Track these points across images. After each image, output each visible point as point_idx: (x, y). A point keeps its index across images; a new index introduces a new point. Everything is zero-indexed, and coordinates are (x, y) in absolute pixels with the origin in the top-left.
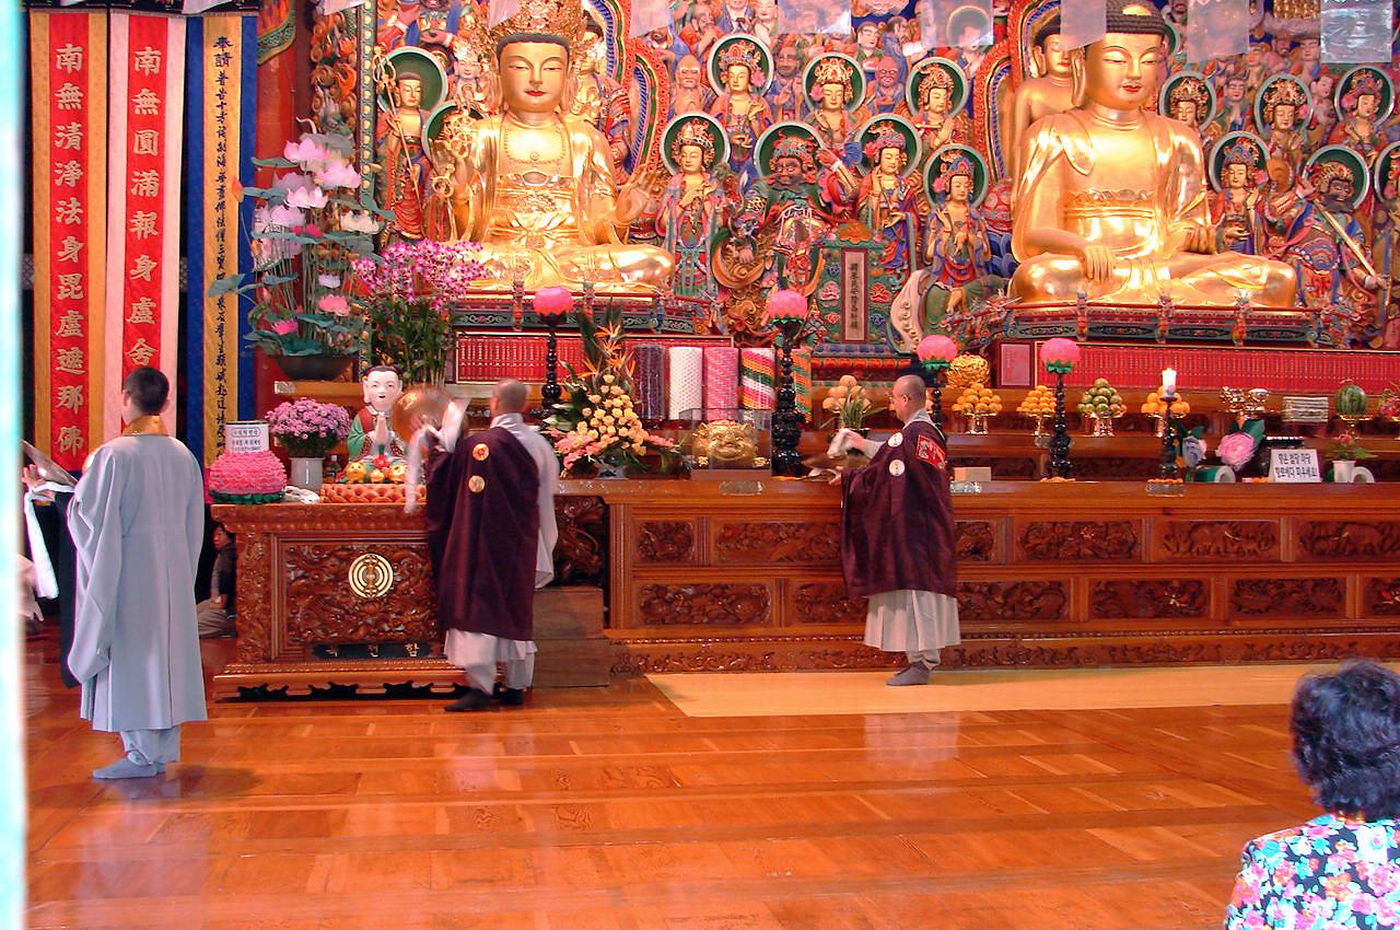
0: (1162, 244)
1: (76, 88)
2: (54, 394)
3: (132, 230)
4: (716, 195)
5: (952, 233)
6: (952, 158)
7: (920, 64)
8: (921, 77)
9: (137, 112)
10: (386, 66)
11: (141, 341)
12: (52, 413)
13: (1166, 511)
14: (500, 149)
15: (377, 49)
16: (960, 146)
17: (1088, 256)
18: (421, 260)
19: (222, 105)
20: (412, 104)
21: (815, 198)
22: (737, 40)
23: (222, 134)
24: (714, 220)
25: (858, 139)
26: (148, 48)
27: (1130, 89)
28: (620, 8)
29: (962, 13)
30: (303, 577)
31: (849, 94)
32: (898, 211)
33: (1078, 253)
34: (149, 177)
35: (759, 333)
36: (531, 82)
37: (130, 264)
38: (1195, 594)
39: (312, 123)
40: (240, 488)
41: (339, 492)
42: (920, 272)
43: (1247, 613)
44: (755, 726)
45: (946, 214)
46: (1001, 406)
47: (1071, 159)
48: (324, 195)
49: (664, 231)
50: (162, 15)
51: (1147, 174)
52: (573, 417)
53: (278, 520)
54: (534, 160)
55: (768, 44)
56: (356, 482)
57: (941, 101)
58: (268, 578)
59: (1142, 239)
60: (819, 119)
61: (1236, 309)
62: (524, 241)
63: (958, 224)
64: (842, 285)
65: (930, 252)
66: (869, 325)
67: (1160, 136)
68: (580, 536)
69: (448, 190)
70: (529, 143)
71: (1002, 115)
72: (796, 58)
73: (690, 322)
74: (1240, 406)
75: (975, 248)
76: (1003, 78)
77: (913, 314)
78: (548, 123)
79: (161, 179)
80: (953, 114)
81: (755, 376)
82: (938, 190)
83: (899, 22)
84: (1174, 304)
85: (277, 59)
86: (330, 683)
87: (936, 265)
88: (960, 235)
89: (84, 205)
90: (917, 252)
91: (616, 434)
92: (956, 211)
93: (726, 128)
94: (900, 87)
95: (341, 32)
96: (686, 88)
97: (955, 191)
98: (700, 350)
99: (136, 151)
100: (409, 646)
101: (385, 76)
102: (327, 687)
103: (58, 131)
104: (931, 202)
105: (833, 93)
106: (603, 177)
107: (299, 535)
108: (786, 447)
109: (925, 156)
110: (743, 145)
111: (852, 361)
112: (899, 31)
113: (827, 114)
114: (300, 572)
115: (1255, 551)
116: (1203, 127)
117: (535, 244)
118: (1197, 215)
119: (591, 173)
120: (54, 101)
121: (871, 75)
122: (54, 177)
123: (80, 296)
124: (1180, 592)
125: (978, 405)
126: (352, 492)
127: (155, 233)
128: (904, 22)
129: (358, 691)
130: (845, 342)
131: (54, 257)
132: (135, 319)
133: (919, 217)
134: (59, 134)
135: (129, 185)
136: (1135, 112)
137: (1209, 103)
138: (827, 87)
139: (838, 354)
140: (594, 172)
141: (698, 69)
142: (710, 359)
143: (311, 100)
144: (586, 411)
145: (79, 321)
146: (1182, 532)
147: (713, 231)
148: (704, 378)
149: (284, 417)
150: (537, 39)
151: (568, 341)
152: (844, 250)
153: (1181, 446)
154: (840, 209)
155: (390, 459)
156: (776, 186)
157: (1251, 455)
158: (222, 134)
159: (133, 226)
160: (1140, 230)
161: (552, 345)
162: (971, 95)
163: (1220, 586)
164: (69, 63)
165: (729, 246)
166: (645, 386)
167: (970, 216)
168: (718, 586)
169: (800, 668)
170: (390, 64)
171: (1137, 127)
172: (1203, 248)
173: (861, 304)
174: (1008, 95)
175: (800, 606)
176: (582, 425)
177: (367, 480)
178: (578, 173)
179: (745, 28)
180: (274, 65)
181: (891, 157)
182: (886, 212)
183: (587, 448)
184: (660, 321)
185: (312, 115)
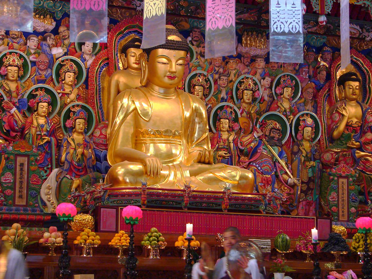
5: (75, 149)
8: (60, 66)
16: (80, 103)
25: (25, 97)
27: (170, 78)
29: (86, 33)
31: (21, 72)
32: (46, 136)
47: (140, 112)
57: (71, 79)
59: (176, 155)
60: (5, 85)
63: (79, 145)
64: (15, 175)
65: (63, 158)
66: (29, 196)
67: (185, 103)
71: (103, 88)
75: (88, 157)
77: (53, 192)
80: (77, 86)
82: (68, 126)
83: (50, 37)
87: (66, 166)
88: (80, 150)
90: (56, 159)
92: (78, 138)
94: (49, 70)
97: (77, 127)
109: (62, 108)
113: (9, 83)
116: (207, 99)
118: (204, 144)
121: (34, 63)
125: (88, 241)
128: (53, 36)
130: (15, 205)
133: (57, 140)
136: (172, 90)
138: (9, 68)
139: (11, 212)
152: (17, 155)
154: (15, 134)
171: (174, 98)
172: (207, 161)
173: (25, 185)
174: (107, 78)
181: (43, 107)
182: (40, 137)
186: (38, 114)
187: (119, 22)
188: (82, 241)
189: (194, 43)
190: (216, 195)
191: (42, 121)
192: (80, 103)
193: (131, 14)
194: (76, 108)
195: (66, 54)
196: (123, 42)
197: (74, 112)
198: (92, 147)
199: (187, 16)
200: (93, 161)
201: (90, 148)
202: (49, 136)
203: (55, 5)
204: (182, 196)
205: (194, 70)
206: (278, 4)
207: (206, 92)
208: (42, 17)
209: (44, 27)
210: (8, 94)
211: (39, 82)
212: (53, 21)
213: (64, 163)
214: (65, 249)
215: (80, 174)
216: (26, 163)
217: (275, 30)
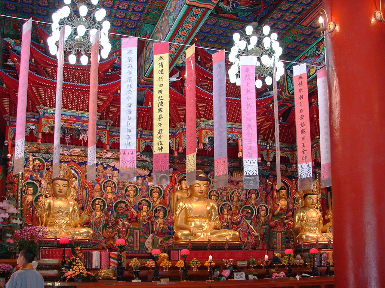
8: (152, 190)
10: (25, 185)
16: (161, 205)
17: (192, 230)
21: (127, 217)
25: (137, 204)
29: (164, 175)
31: (135, 194)
45: (158, 221)
49: (91, 224)
51: (205, 212)
52: (69, 268)
57: (157, 195)
59: (204, 226)
62: (57, 226)
63: (161, 223)
64: (134, 237)
65: (154, 229)
69: (39, 214)
71: (171, 199)
72: (123, 185)
74: (227, 263)
77: (150, 244)
78: (64, 199)
81: (113, 258)
83: (147, 177)
87: (156, 233)
88: (161, 226)
91: (79, 272)
93: (106, 201)
97: (160, 216)
98: (100, 252)
101: (24, 187)
105: (131, 193)
112: (147, 180)
113: (130, 198)
116: (217, 201)
117: (60, 227)
128: (148, 177)
133: (152, 222)
136: (202, 198)
150: (61, 180)
152: (134, 229)
161: (64, 251)
174: (173, 194)
176: (71, 270)
178: (71, 210)
181: (145, 208)
182: (144, 221)
184: (90, 246)
185: (6, 196)
187: (177, 170)
189: (211, 177)
191: (145, 214)
192: (161, 205)
193: (183, 166)
197: (159, 210)
199: (208, 165)
206: (247, 163)
211: (143, 197)
213: (155, 231)
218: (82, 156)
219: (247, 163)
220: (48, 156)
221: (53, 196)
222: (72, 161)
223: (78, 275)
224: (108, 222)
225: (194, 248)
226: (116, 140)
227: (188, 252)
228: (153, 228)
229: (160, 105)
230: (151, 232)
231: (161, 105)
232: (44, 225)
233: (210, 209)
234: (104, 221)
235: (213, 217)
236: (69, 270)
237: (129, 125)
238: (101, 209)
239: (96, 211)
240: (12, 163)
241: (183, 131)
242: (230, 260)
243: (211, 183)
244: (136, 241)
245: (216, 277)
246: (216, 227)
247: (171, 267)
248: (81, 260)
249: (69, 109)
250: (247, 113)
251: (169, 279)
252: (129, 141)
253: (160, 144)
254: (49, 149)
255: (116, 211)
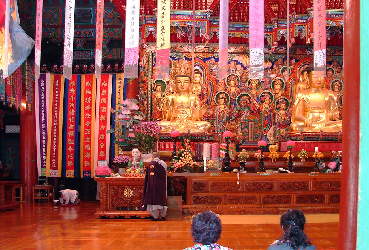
0: (326, 118)
1: (90, 90)
2: (84, 154)
3: (101, 119)
4: (227, 109)
5: (281, 117)
6: (282, 100)
7: (274, 79)
8: (274, 82)
9: (102, 94)
10: (154, 83)
11: (102, 143)
12: (84, 158)
13: (315, 179)
14: (174, 101)
15: (152, 79)
16: (283, 97)
17: (305, 121)
18: (148, 125)
19: (119, 93)
20: (160, 91)
21: (249, 110)
22: (232, 75)
23: (119, 99)
24: (227, 115)
25: (260, 96)
26: (105, 81)
27: (319, 84)
28: (206, 69)
29: (283, 68)
30: (114, 193)
31: (258, 86)
32: (269, 112)
33: (304, 122)
34: (104, 108)
35: (237, 140)
36: (181, 86)
37: (100, 127)
38: (322, 198)
39: (139, 96)
40: (100, 174)
41: (128, 175)
42: (274, 126)
43: (334, 202)
44: (252, 226)
45: (280, 113)
46: (279, 156)
47: (305, 100)
48: (130, 112)
49: (215, 118)
50: (92, 74)
51: (323, 103)
52: (178, 159)
53: (108, 181)
54: (182, 103)
55: (239, 75)
56: (128, 173)
57: (279, 87)
58: (107, 193)
59: (321, 117)
60: (251, 92)
61: (338, 133)
62: (179, 121)
63: (283, 115)
64: (249, 129)
65: (276, 121)
66: (255, 138)
67: (326, 94)
68: (180, 185)
69: (161, 110)
70: (182, 99)
71: (294, 90)
72: (245, 79)
73: (214, 138)
74: (335, 155)
75: (287, 120)
76: (294, 82)
77: (272, 136)
78: (186, 94)
79: (107, 109)
80: (282, 90)
81: (223, 150)
82: (278, 107)
83: (269, 70)
84: (323, 132)
85: (131, 82)
86: (150, 216)
87: (277, 124)
88: (283, 117)
89: (91, 114)
90: (273, 121)
91: (187, 163)
92: (282, 112)
93: (230, 94)
94: (270, 84)
95: (144, 76)
96: (221, 86)
97: (282, 108)
98: (210, 144)
99: (102, 103)
100: (136, 208)
101: (154, 85)
102: (149, 216)
103: (86, 99)
104: (277, 110)
105: (254, 86)
106: (198, 106)
107: (116, 184)
108: (226, 166)
109: (275, 100)
110: (233, 98)
111: (250, 146)
112: (269, 72)
113: (252, 91)
114: (114, 192)
115: (336, 188)
116: (340, 92)
117: (181, 121)
118: (335, 112)
119: (195, 105)
120: (85, 93)
121: (263, 82)
122: (85, 109)
123: (90, 134)
124: (318, 198)
125: (273, 156)
126: (127, 175)
127: (105, 120)
128: (271, 70)
129: (124, 217)
130: (249, 142)
131: (84, 125)
132: (101, 138)
133: (273, 113)
134: (86, 100)
135: (100, 110)
136: (320, 89)
137: (342, 86)
138: (253, 85)
139: (254, 145)
140: (196, 105)
141: (223, 82)
142: (212, 146)
143: (139, 91)
144: (181, 158)
145: (89, 139)
146: (317, 183)
147: (226, 117)
148: (211, 150)
149: (116, 159)
150: (183, 76)
151: (179, 142)
152: (249, 121)
153: (319, 164)
154: (256, 112)
155: (136, 168)
156: (241, 107)
157: (336, 166)
158: (119, 99)
159: (101, 118)
160: (321, 116)
161: (175, 143)
162: (286, 86)
163: (327, 196)
164: (89, 85)
165: (230, 121)
166: (198, 152)
167: (285, 113)
168: (211, 196)
169: (228, 214)
170: (155, 82)
171: (321, 92)
172: (334, 119)
173: (253, 134)
174: (295, 85)
175: (229, 200)
176: (180, 161)
177: (130, 173)
178: (192, 105)
179: (234, 72)
180: (131, 83)
181: (267, 100)
182: (266, 113)
183: (180, 166)
184: (205, 138)
185: (139, 94)
186: (265, 103)
187: (299, 61)
188: (271, 156)
189: (334, 67)
190: (336, 134)
191: (267, 106)
192: (283, 97)
193: (305, 57)
194: (281, 100)
195: (276, 77)
196: (302, 69)
197: (281, 101)
198: (289, 116)
199: (330, 55)
200: (289, 122)
201: (288, 116)
202: (270, 112)
203: (271, 56)
204: (319, 135)
205: (334, 79)
206: (253, 53)
207: (340, 88)
208: (266, 62)
209: (267, 66)
210: (252, 96)
211: (265, 89)
212: (271, 63)
213: (276, 123)
214: (261, 159)
215: (284, 127)
216: (253, 124)
217: (252, 65)
218: (206, 53)
219: (253, 53)
220: (175, 55)
221: (177, 92)
222: (197, 58)
223: (185, 166)
224: (231, 115)
225: (306, 139)
226: (232, 35)
227: (293, 143)
228: (275, 120)
229: (163, 3)
230: (272, 124)
231: (164, 3)
232: (166, 119)
233: (328, 100)
234: (227, 114)
235: (331, 108)
236: (178, 162)
237: (133, 25)
238: (224, 103)
239: (220, 105)
240: (143, 64)
241: (295, 22)
242: (339, 152)
243: (334, 73)
244: (251, 132)
245: (321, 169)
246: (332, 118)
247: (279, 158)
248: (189, 152)
249: (183, 9)
250: (255, 2)
251: (272, 170)
252: (132, 40)
253: (162, 40)
254: (176, 48)
255: (239, 104)
